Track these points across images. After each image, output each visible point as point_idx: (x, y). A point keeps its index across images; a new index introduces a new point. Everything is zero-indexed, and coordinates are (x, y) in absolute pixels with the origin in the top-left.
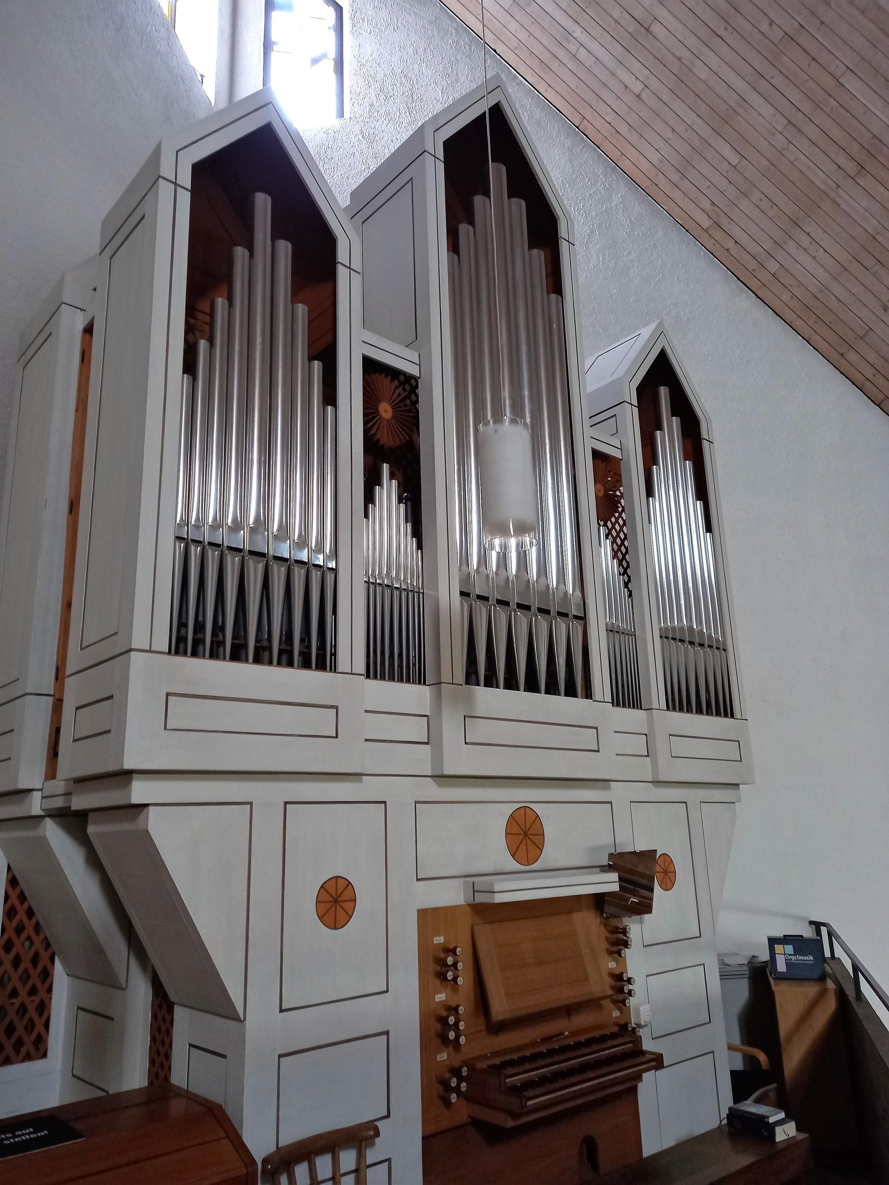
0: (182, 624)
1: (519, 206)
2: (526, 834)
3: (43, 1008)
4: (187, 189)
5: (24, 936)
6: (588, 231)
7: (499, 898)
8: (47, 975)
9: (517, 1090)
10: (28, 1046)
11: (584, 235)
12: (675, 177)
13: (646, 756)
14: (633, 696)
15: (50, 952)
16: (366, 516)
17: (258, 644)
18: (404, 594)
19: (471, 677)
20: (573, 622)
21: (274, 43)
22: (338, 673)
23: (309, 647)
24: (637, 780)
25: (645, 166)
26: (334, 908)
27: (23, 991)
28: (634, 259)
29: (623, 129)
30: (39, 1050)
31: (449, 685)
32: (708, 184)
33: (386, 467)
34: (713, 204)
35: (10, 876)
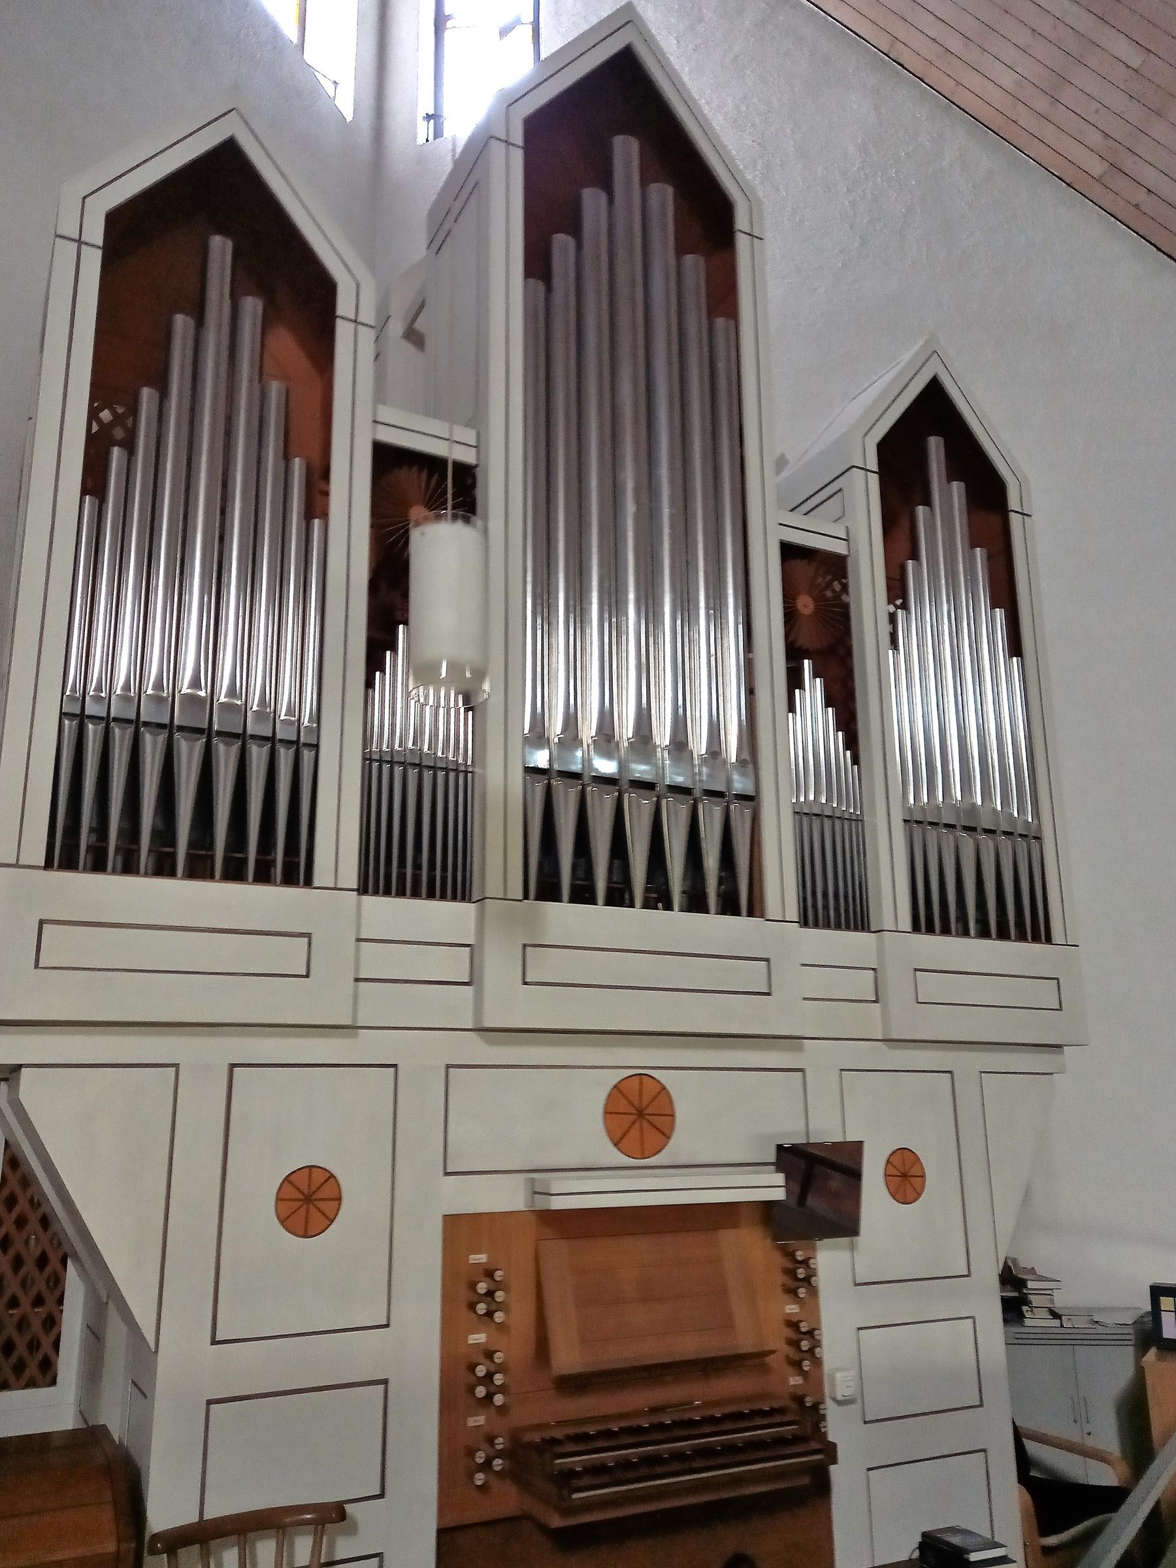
1: (663, 195)
2: (641, 1114)
3: (52, 1323)
4: (741, 231)
7: (558, 1204)
8: (57, 1282)
9: (567, 1478)
10: (32, 1369)
12: (1041, 103)
15: (60, 1254)
18: (441, 775)
21: (448, 18)
22: (315, 888)
24: (946, 1039)
25: (993, 94)
27: (25, 1301)
29: (955, 43)
30: (46, 1374)
31: (501, 901)
32: (1095, 105)
34: (1107, 136)
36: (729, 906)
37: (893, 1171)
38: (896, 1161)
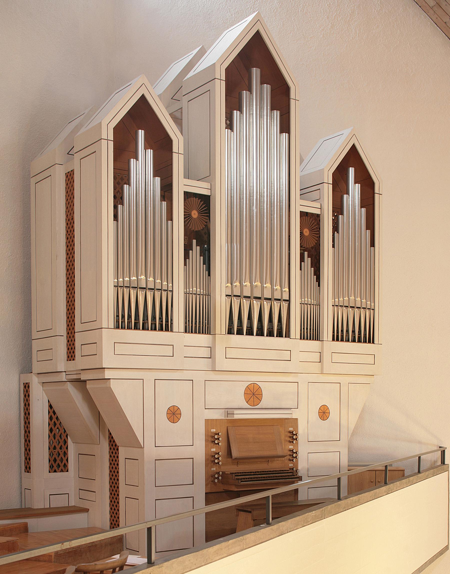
0: (118, 316)
5: (56, 427)
6: (350, 12)
10: (62, 467)
11: (348, 15)
13: (319, 362)
14: (313, 334)
16: (230, 126)
17: (144, 322)
19: (230, 332)
20: (283, 303)
23: (162, 321)
26: (173, 416)
27: (58, 448)
28: (381, 31)
33: (194, 241)
35: (49, 404)
36: (280, 335)
37: (320, 411)
38: (322, 409)
